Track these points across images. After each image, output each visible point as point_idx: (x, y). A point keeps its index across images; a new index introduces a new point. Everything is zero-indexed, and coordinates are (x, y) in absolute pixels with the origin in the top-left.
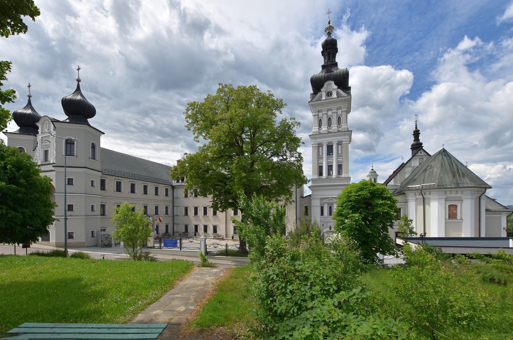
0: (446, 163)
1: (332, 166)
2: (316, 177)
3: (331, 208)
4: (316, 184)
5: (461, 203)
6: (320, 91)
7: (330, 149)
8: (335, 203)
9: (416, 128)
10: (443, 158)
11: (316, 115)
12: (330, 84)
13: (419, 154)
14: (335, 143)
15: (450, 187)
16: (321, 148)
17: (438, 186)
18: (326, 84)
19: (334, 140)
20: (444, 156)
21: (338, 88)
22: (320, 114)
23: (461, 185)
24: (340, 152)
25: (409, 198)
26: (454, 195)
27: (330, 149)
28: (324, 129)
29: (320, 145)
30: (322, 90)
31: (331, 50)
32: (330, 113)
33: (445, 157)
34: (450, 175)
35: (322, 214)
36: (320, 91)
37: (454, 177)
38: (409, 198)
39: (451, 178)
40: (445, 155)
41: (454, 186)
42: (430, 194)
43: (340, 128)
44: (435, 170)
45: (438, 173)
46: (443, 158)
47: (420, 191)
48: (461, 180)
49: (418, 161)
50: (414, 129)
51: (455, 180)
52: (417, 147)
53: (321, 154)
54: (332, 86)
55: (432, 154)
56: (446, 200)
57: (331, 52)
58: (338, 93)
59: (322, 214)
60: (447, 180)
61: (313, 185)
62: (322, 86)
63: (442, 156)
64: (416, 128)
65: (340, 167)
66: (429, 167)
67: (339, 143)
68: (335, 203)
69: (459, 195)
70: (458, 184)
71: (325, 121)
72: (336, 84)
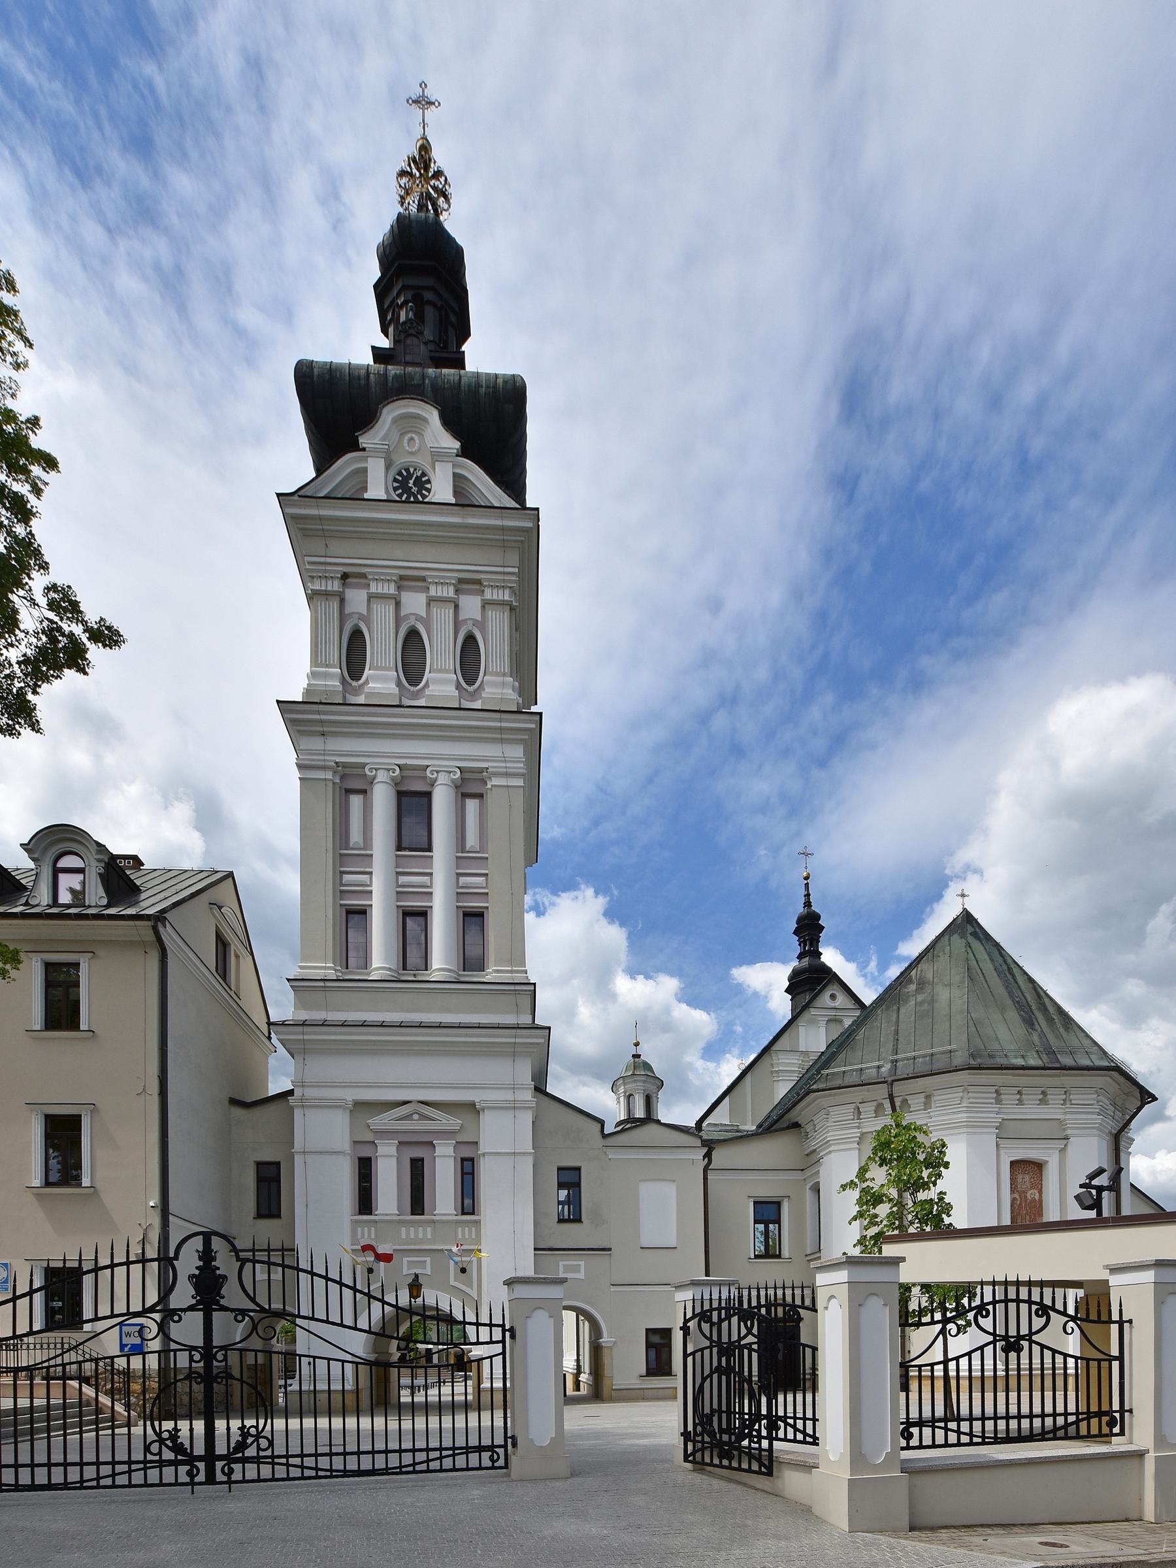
0: (988, 966)
1: (423, 914)
2: (324, 968)
3: (417, 1172)
4: (319, 1015)
5: (1063, 1151)
6: (355, 447)
7: (413, 803)
8: (446, 1134)
9: (808, 904)
10: (969, 945)
11: (326, 594)
12: (413, 424)
13: (825, 999)
14: (442, 778)
15: (1020, 1062)
16: (356, 801)
17: (972, 1056)
18: (390, 414)
19: (442, 759)
20: (971, 939)
21: (465, 452)
22: (357, 599)
23: (1066, 1060)
24: (472, 840)
25: (831, 1135)
26: (1031, 1110)
27: (413, 803)
28: (380, 680)
29: (350, 784)
30: (364, 441)
31: (429, 281)
32: (414, 603)
33: (976, 944)
34: (1013, 1015)
35: (365, 1202)
36: (355, 447)
37: (1030, 1022)
38: (831, 1135)
39: (1021, 1030)
40: (975, 935)
41: (1039, 1063)
42: (927, 1104)
43: (474, 696)
44: (943, 994)
45: (960, 1004)
46: (969, 945)
47: (883, 1090)
48: (1059, 1037)
49: (823, 1030)
50: (800, 909)
51: (1036, 1038)
52: (810, 982)
53: (356, 836)
54: (424, 437)
55: (867, 1002)
56: (1004, 1134)
57: (428, 296)
58: (460, 483)
59: (365, 1202)
60: (1003, 1033)
61: (303, 1016)
62: (368, 419)
63: (963, 936)
64: (808, 904)
65: (472, 919)
66: (913, 987)
67: (469, 787)
68: (446, 1134)
69: (1053, 1111)
70: (1051, 1053)
71: (383, 648)
72: (448, 422)
